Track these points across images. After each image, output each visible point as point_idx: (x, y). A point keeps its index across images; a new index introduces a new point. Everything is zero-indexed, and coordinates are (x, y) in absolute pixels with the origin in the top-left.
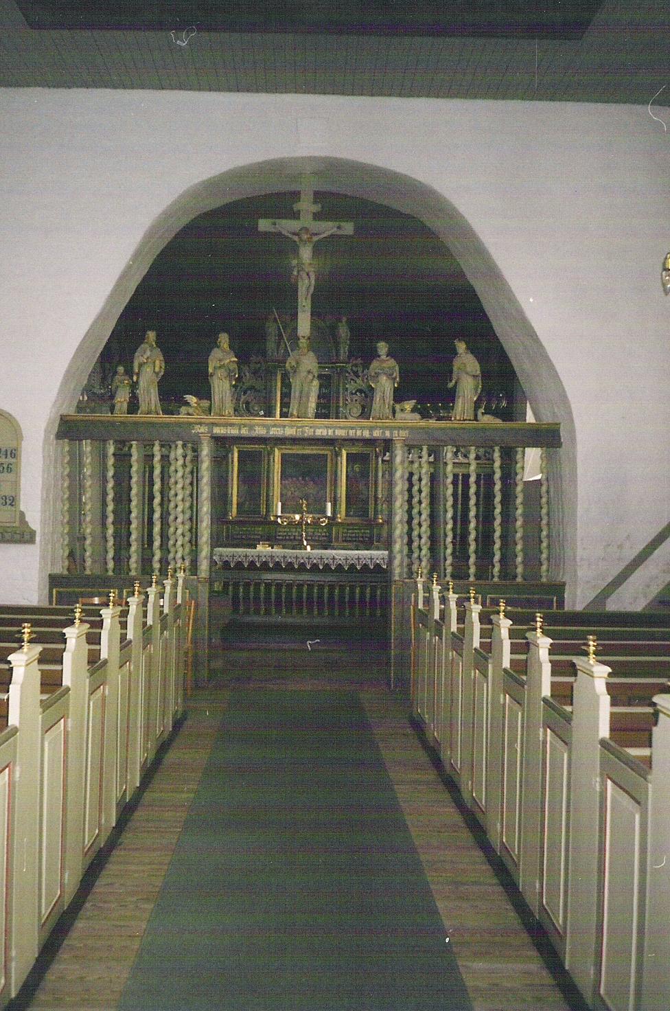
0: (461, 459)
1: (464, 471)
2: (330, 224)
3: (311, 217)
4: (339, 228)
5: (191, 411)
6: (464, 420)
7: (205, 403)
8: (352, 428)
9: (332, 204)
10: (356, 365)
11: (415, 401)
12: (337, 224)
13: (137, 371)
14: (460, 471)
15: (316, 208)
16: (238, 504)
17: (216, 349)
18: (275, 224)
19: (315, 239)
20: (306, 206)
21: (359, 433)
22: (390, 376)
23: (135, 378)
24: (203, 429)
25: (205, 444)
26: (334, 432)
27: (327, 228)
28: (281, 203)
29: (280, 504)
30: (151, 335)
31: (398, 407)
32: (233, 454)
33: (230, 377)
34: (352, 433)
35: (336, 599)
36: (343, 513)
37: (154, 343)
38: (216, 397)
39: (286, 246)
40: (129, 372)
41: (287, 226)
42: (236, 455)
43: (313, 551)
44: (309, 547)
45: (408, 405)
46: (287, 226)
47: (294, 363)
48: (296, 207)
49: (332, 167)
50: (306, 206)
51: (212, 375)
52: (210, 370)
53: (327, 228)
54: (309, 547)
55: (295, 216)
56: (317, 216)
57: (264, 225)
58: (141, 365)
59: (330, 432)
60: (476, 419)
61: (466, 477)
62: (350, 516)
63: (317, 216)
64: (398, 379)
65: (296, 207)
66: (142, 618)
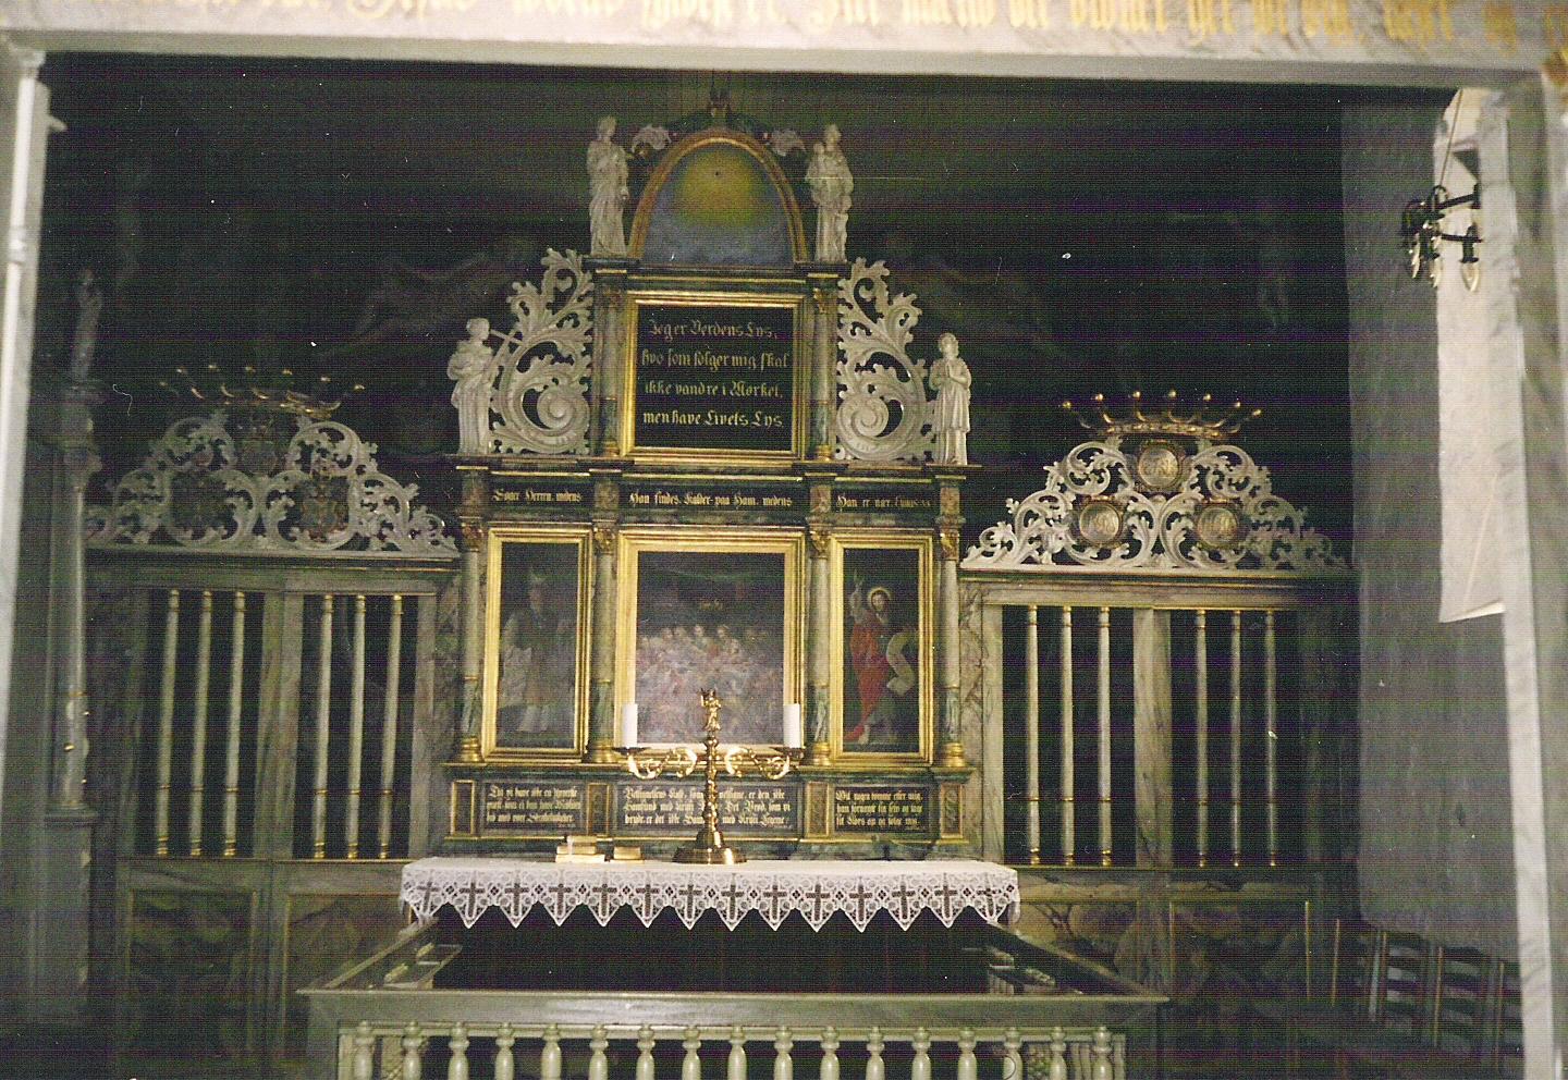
30: (833, 134)
32: (484, 554)
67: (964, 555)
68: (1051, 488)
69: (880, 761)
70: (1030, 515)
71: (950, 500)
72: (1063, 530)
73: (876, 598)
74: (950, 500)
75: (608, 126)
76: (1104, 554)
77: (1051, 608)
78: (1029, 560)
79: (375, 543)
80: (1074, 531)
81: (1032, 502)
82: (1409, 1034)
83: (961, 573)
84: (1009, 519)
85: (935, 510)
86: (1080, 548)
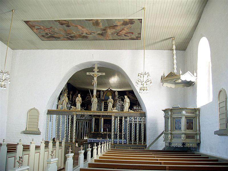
0: (135, 120)
7: (75, 108)
9: (100, 69)
10: (119, 100)
14: (135, 123)
15: (98, 70)
16: (94, 129)
17: (77, 97)
19: (97, 76)
20: (96, 70)
21: (105, 114)
24: (74, 113)
27: (100, 74)
28: (91, 70)
34: (104, 114)
38: (77, 107)
39: (92, 77)
42: (94, 119)
46: (92, 74)
48: (94, 70)
49: (101, 63)
50: (96, 70)
53: (100, 74)
54: (108, 139)
55: (94, 72)
56: (98, 72)
57: (88, 74)
59: (99, 114)
60: (129, 111)
62: (96, 131)
63: (98, 72)
65: (94, 70)
66: (6, 143)
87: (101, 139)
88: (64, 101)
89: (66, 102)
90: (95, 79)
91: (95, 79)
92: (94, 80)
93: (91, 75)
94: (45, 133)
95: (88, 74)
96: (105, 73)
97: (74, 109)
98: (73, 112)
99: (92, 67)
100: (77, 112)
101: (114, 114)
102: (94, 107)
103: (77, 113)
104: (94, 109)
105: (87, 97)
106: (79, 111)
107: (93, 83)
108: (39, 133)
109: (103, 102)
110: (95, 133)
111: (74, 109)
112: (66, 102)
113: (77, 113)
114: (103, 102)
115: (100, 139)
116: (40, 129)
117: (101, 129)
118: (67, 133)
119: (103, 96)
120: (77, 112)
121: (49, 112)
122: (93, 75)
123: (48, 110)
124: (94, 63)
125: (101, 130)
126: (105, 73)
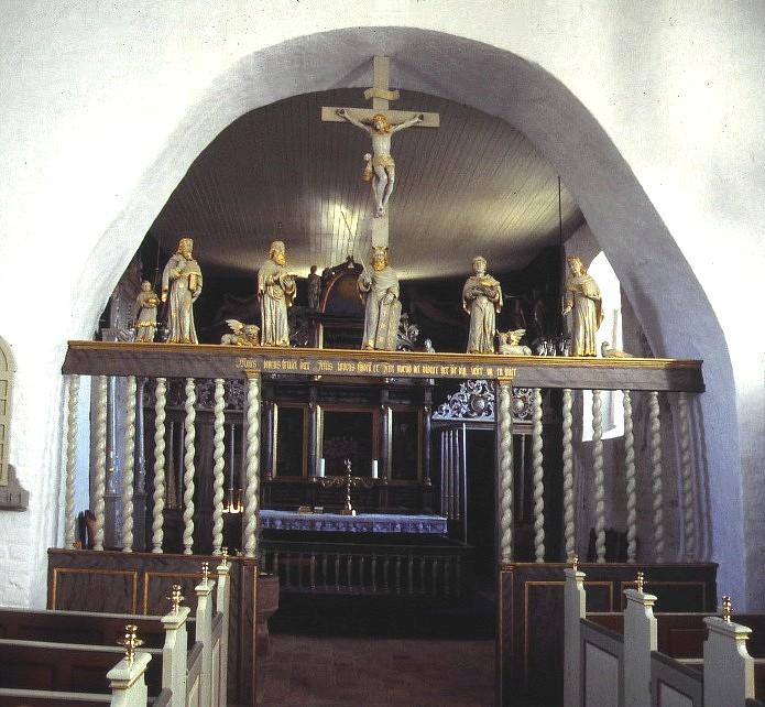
1: (528, 432)
2: (410, 114)
3: (387, 105)
4: (422, 117)
5: (235, 339)
6: (588, 355)
7: (253, 329)
8: (444, 364)
11: (521, 332)
12: (419, 114)
13: (167, 287)
15: (390, 96)
18: (342, 112)
19: (393, 129)
21: (453, 371)
22: (490, 298)
23: (164, 296)
24: (249, 364)
25: (254, 384)
26: (421, 369)
27: (408, 119)
29: (323, 461)
30: (187, 244)
31: (504, 337)
32: (273, 412)
33: (288, 297)
35: (435, 575)
36: (390, 475)
37: (190, 254)
40: (158, 290)
41: (356, 115)
42: (276, 412)
43: (360, 516)
44: (354, 512)
45: (516, 335)
46: (356, 115)
47: (369, 280)
51: (262, 295)
52: (261, 287)
53: (408, 119)
54: (354, 512)
56: (393, 106)
57: (328, 114)
58: (172, 281)
59: (416, 369)
61: (530, 440)
63: (393, 106)
64: (501, 303)
67: (433, 414)
68: (462, 392)
69: (404, 483)
70: (455, 401)
71: (428, 396)
72: (466, 406)
73: (403, 428)
74: (428, 396)
75: (187, 244)
76: (480, 415)
77: (517, 435)
78: (455, 416)
79: (237, 407)
80: (470, 407)
81: (456, 397)
82: (277, 579)
83: (431, 420)
84: (448, 402)
85: (308, 395)
86: (472, 412)
87: (318, 512)
88: (181, 285)
89: (192, 292)
90: (383, 145)
91: (383, 145)
92: (373, 153)
93: (348, 122)
94: (52, 499)
95: (328, 114)
96: (437, 115)
97: (249, 337)
98: (242, 360)
99: (344, 86)
100: (265, 355)
101: (510, 372)
102: (382, 326)
103: (268, 365)
104: (381, 340)
105: (224, 308)
106: (282, 354)
107: (369, 168)
108: (14, 501)
109: (321, 327)
110: (283, 483)
111: (249, 337)
112: (192, 292)
113: (268, 365)
114: (321, 327)
115: (313, 510)
116: (20, 475)
117: (320, 464)
118: (141, 483)
119: (321, 297)
120: (265, 355)
121: (79, 359)
122: (367, 123)
123: (69, 342)
124: (364, 54)
125: (312, 468)
126: (437, 115)
